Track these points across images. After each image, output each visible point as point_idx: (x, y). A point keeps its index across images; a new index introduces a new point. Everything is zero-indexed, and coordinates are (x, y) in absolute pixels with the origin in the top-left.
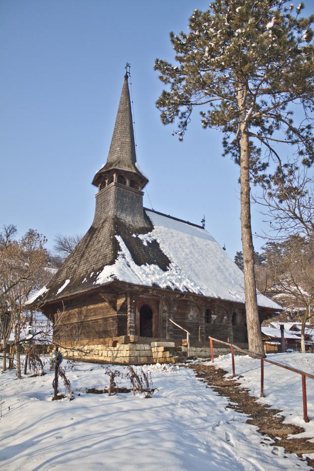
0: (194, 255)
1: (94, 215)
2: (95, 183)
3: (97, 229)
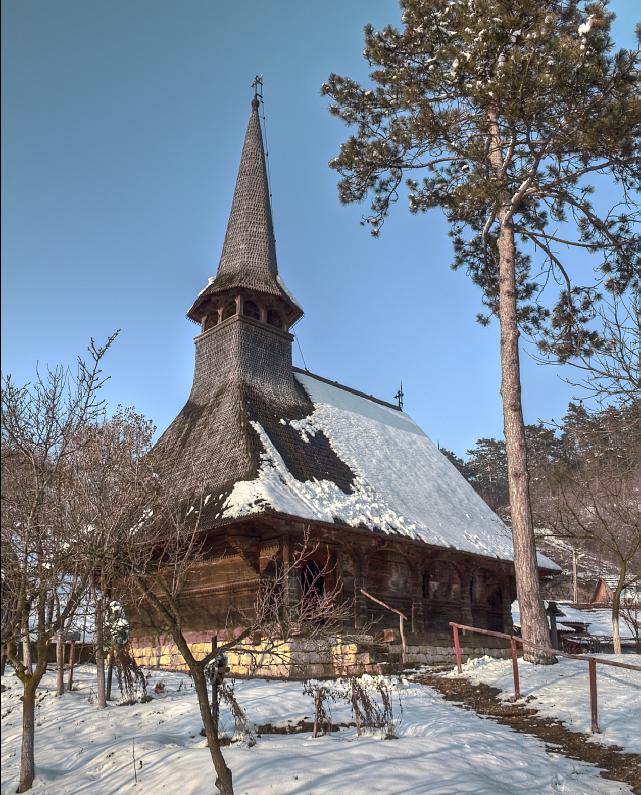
0: (391, 462)
1: (192, 378)
2: (195, 314)
3: (204, 407)
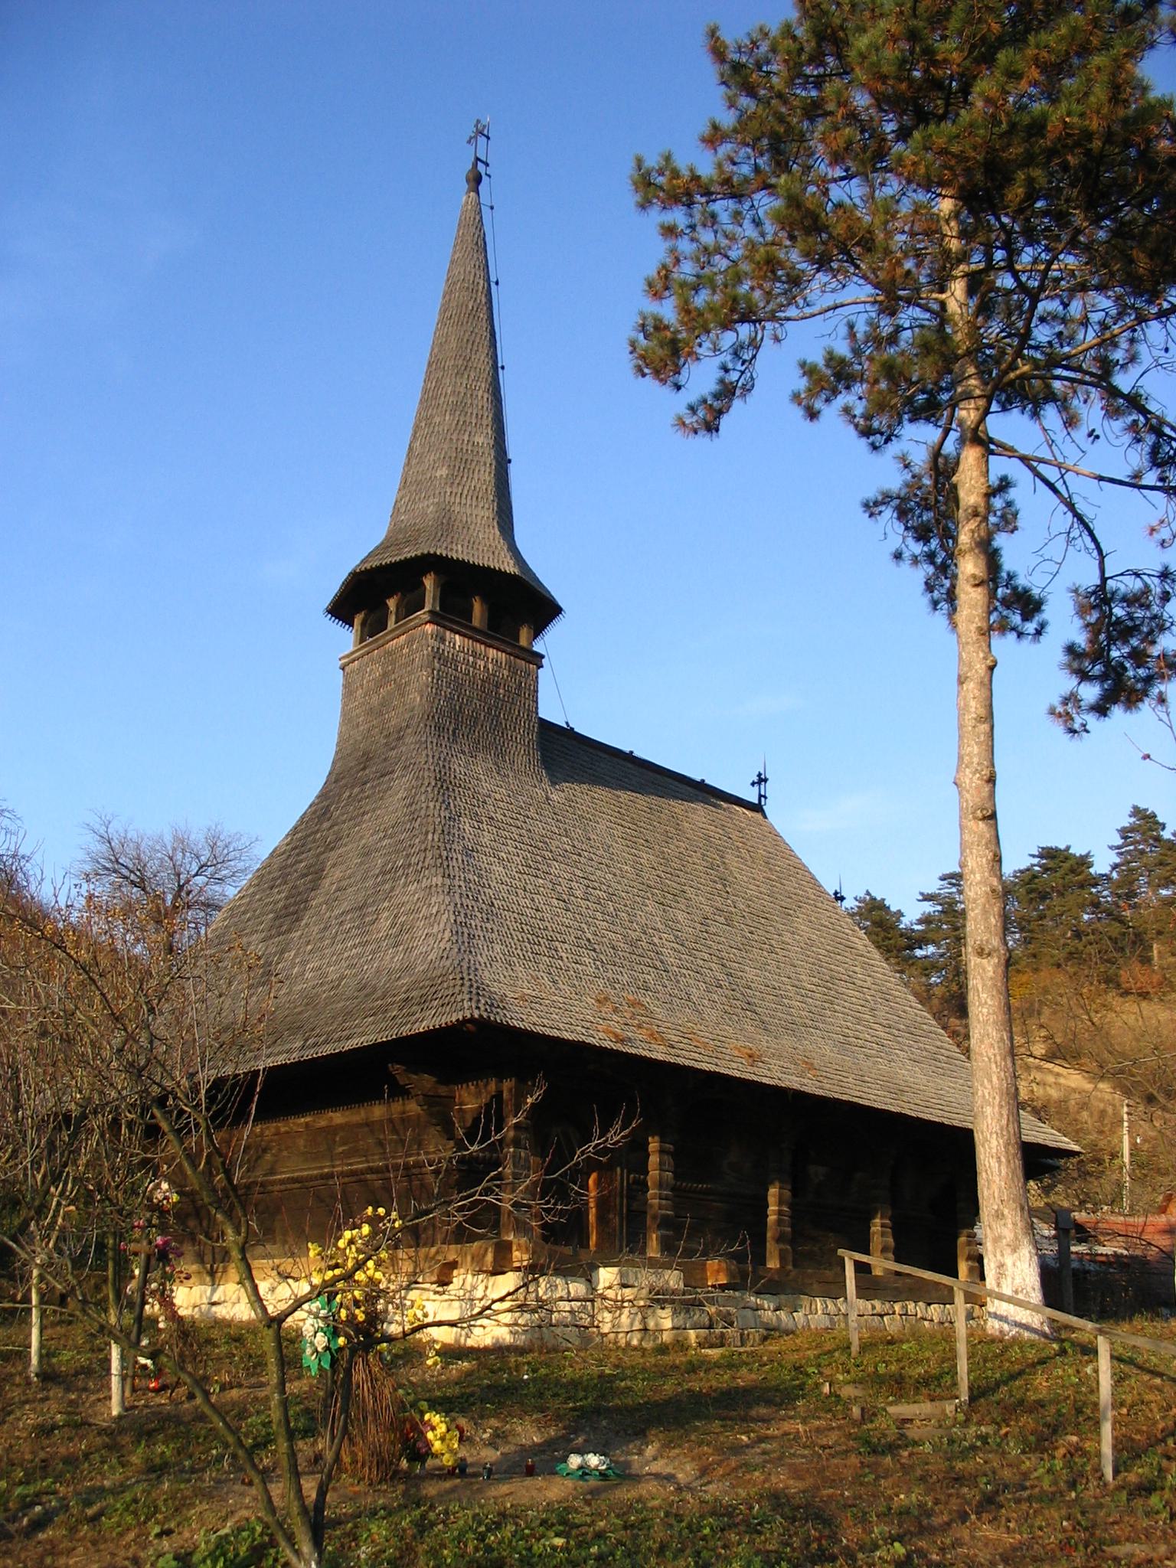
2: (342, 609)
